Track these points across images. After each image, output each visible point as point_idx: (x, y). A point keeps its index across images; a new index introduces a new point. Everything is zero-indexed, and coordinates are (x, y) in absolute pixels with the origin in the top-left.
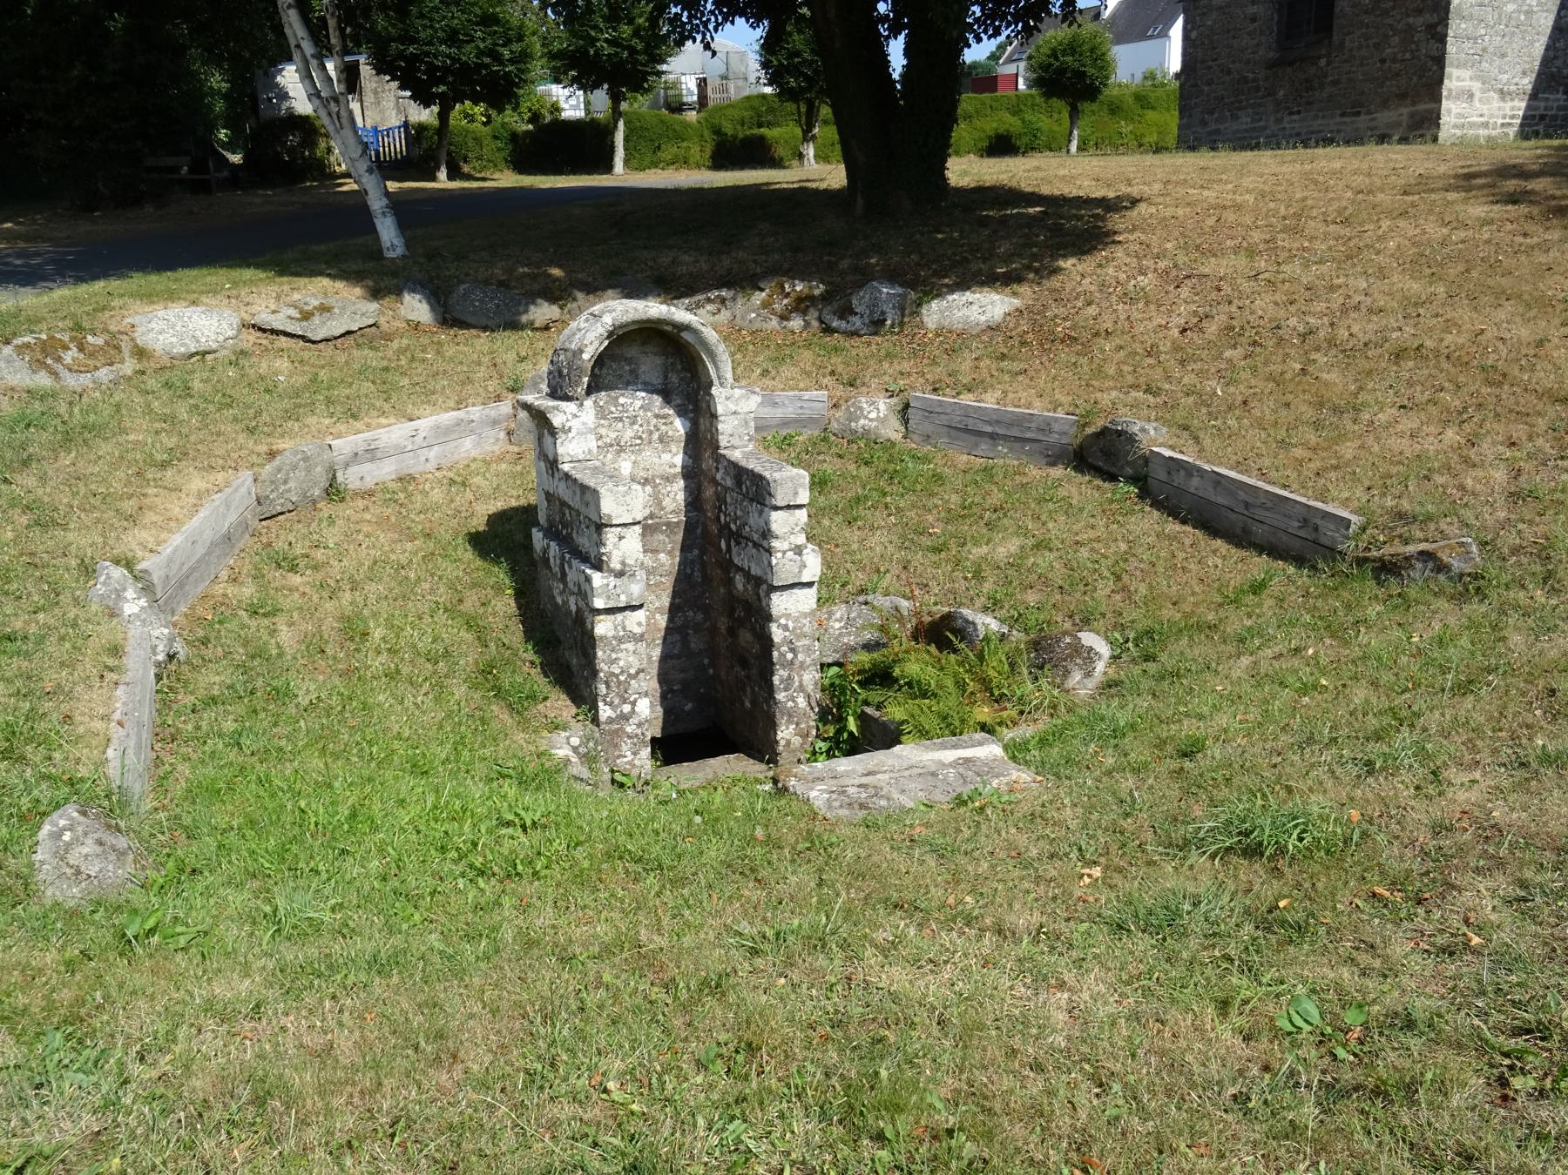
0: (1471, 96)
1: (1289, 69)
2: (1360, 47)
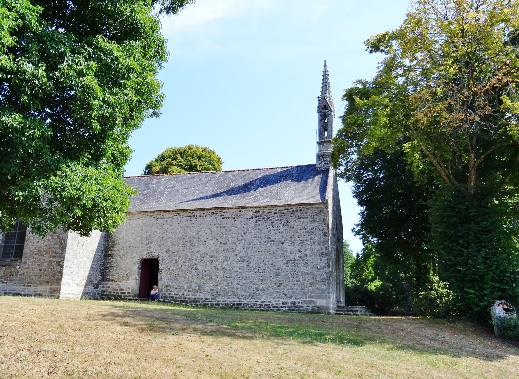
0: (69, 285)
1: (3, 268)
2: (32, 265)
